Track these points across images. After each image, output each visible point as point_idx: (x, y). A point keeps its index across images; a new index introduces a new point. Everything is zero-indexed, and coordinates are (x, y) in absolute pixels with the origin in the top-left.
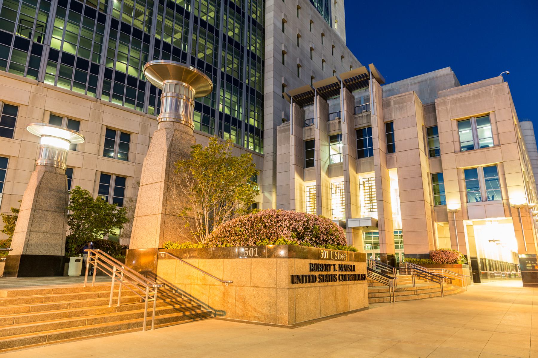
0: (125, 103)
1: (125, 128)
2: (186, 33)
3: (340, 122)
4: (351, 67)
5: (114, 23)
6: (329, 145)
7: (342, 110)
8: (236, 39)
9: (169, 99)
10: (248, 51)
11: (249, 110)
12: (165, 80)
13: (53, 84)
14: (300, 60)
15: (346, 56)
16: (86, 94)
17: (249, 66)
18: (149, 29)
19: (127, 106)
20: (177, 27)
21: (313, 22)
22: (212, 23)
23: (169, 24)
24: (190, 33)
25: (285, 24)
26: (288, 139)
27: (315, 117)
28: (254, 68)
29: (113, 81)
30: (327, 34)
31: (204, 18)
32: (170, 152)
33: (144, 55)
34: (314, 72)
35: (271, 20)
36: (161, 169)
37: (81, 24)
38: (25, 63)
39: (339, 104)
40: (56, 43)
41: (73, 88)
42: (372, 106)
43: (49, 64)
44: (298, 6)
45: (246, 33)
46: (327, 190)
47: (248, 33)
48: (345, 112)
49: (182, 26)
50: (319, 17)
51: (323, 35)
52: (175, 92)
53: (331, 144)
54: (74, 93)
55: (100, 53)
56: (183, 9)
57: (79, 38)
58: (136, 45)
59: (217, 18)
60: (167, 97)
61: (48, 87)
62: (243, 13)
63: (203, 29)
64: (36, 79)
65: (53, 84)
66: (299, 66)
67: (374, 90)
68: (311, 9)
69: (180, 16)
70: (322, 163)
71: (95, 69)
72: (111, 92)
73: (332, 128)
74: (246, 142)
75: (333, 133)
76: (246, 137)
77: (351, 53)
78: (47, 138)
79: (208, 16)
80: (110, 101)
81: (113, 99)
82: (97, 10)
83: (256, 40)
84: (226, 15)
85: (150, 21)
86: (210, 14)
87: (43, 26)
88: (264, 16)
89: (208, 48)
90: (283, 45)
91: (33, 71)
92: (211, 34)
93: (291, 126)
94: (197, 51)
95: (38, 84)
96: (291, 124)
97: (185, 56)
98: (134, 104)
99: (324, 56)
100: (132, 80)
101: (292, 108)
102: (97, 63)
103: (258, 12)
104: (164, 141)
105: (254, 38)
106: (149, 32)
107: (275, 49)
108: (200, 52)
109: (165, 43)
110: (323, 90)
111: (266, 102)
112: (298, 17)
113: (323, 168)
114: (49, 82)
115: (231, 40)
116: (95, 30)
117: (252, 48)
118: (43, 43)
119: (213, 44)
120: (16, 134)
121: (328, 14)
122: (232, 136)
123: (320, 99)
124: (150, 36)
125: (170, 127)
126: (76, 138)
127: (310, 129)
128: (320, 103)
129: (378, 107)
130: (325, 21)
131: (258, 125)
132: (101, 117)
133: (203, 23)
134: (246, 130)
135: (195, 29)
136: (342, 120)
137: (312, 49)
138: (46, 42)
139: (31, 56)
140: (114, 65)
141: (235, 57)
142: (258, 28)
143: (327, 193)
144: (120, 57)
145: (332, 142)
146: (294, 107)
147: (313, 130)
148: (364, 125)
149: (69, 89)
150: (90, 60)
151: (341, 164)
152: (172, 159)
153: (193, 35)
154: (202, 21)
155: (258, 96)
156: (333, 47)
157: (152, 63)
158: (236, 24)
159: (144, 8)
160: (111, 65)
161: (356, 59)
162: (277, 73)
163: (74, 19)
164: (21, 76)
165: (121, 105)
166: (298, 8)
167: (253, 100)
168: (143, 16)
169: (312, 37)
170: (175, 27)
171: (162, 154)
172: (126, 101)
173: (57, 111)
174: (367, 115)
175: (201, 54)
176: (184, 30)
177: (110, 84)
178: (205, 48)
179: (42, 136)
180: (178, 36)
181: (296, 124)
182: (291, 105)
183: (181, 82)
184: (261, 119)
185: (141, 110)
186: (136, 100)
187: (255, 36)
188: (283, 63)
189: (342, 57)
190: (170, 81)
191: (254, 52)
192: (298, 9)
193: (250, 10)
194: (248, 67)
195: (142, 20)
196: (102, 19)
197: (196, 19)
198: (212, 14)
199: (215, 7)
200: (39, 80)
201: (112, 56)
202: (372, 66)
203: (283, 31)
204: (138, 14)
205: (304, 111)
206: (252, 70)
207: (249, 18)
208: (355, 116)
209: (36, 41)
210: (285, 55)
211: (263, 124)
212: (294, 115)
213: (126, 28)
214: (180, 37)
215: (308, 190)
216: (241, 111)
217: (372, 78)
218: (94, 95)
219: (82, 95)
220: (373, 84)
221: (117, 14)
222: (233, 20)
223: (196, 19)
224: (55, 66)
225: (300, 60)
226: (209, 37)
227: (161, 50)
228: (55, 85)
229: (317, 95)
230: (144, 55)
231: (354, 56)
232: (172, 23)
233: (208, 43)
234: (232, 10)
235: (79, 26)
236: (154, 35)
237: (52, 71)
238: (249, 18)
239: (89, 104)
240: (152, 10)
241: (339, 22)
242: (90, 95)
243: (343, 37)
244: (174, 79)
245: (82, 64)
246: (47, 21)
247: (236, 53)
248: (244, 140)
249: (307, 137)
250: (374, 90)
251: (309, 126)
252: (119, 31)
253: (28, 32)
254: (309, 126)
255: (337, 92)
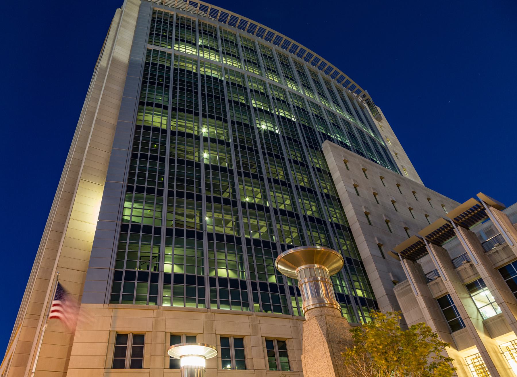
0: (232, 307)
1: (238, 333)
2: (270, 225)
3: (471, 265)
4: (443, 206)
5: (210, 236)
6: (471, 297)
7: (468, 251)
8: (316, 215)
9: (307, 285)
11: (352, 282)
12: (298, 267)
13: (169, 305)
14: (386, 216)
15: (431, 197)
16: (197, 307)
19: (235, 309)
20: (261, 223)
21: (383, 178)
24: (274, 225)
25: (358, 188)
26: (415, 302)
28: (342, 237)
29: (218, 288)
30: (402, 183)
32: (329, 342)
33: (239, 256)
35: (342, 189)
37: (185, 246)
38: (146, 292)
39: (460, 244)
40: (168, 268)
41: (186, 304)
43: (165, 288)
46: (498, 357)
47: (326, 207)
48: (473, 252)
49: (265, 221)
50: (387, 172)
51: (398, 185)
52: (311, 276)
53: (472, 295)
54: (188, 308)
55: (203, 265)
57: (185, 257)
58: (231, 249)
59: (293, 203)
60: (305, 283)
61: (166, 309)
62: (315, 192)
63: (285, 217)
64: (156, 304)
65: (169, 305)
66: (387, 222)
67: (498, 218)
68: (376, 167)
70: (474, 321)
72: (218, 299)
73: (464, 276)
74: (361, 318)
75: (468, 281)
76: (359, 312)
77: (436, 193)
78: (186, 357)
80: (219, 308)
81: (221, 306)
82: (195, 230)
83: (335, 211)
84: (301, 198)
85: (238, 225)
86: (286, 203)
87: (156, 257)
88: (335, 188)
89: (293, 232)
90: (363, 207)
91: (154, 298)
92: (292, 219)
93: (412, 286)
94: (284, 238)
95: (158, 309)
96: (410, 282)
98: (240, 305)
99: (409, 204)
100: (234, 282)
101: (406, 266)
102: (202, 275)
104: (318, 331)
105: (333, 210)
106: (239, 234)
107: (356, 214)
108: (286, 238)
109: (255, 240)
111: (367, 268)
112: (367, 178)
113: (477, 327)
114: (166, 305)
115: (311, 219)
116: (196, 247)
117: (334, 219)
118: (158, 271)
119: (296, 227)
120: (145, 364)
121: (393, 166)
122: (344, 315)
124: (240, 238)
125: (319, 314)
126: (210, 352)
127: (436, 283)
128: (436, 251)
130: (393, 172)
131: (367, 295)
132: (214, 327)
133: (283, 212)
134: (357, 304)
135: (277, 220)
136: (474, 262)
137: (393, 202)
138: (160, 270)
139: (151, 285)
141: (321, 233)
142: (333, 200)
144: (220, 265)
145: (472, 292)
146: (406, 264)
147: (441, 284)
148: (506, 261)
150: (196, 274)
152: (334, 350)
153: (277, 225)
154: (281, 210)
156: (414, 193)
157: (283, 255)
159: (230, 216)
160: (213, 274)
161: (444, 197)
163: (179, 244)
164: (144, 305)
165: (229, 309)
166: (364, 171)
167: (352, 269)
168: (231, 223)
170: (260, 224)
173: (176, 330)
174: (503, 249)
176: (268, 223)
177: (216, 291)
178: (291, 233)
179: (181, 357)
180: (264, 230)
182: (401, 262)
183: (312, 265)
184: (368, 287)
185: (247, 310)
186: (241, 301)
187: (333, 208)
188: (370, 224)
189: (429, 199)
191: (337, 222)
192: (364, 172)
193: (320, 187)
194: (336, 239)
195: (232, 226)
196: (200, 236)
197: (275, 210)
198: (288, 202)
199: (288, 195)
200: (159, 305)
201: (214, 265)
203: (358, 195)
204: (227, 222)
207: (322, 194)
209: (152, 270)
210: (369, 216)
211: (372, 292)
213: (220, 237)
214: (266, 230)
215: (469, 362)
216: (344, 284)
217: (488, 207)
218: (204, 306)
220: (492, 213)
221: (211, 229)
222: (308, 200)
223: (275, 210)
225: (386, 216)
226: (292, 222)
227: (253, 247)
228: (172, 305)
229: (428, 243)
230: (239, 256)
231: (440, 195)
232: (256, 221)
233: (291, 228)
234: (305, 193)
235: (183, 248)
236: (244, 236)
237: (167, 294)
238: (322, 194)
239: (202, 317)
240: (238, 216)
241: (407, 170)
242: (201, 306)
243: (419, 181)
244: (307, 264)
245: (191, 279)
247: (320, 229)
248: (359, 317)
250: (498, 218)
251: (432, 280)
252: (215, 242)
253: (146, 265)
254: (432, 280)
255: (451, 233)
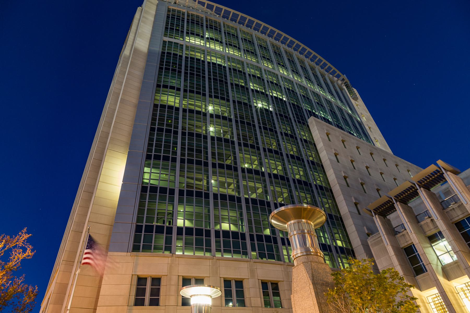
0: (234, 255)
2: (265, 187)
3: (432, 220)
4: (408, 171)
6: (432, 246)
7: (429, 208)
8: (303, 179)
9: (296, 236)
10: (316, 185)
13: (181, 253)
15: (399, 163)
17: (320, 197)
18: (239, 193)
19: (236, 256)
20: (258, 185)
22: (281, 173)
23: (252, 185)
24: (268, 186)
25: (338, 156)
27: (404, 222)
30: (374, 152)
31: (275, 172)
34: (377, 185)
35: (325, 157)
36: (312, 303)
37: (194, 204)
40: (180, 222)
41: (195, 252)
42: (459, 196)
43: (177, 239)
44: (342, 140)
45: (310, 173)
46: (454, 296)
47: (311, 172)
48: (434, 209)
49: (261, 183)
50: (363, 143)
51: (371, 154)
52: (299, 229)
53: (433, 245)
54: (197, 256)
55: (209, 220)
56: (259, 171)
57: (194, 214)
58: (233, 207)
59: (284, 169)
60: (294, 235)
61: (179, 257)
62: (303, 160)
63: (277, 181)
64: (171, 253)
65: (181, 253)
68: (353, 139)
69: (258, 177)
70: (434, 267)
71: (208, 233)
72: (222, 249)
73: (426, 229)
74: (341, 264)
75: (430, 233)
76: (339, 259)
77: (403, 160)
78: (196, 297)
79: (277, 170)
82: (203, 191)
85: (238, 187)
87: (171, 213)
90: (342, 172)
94: (277, 198)
96: (381, 234)
97: (268, 204)
98: (240, 253)
99: (381, 169)
100: (235, 234)
101: (377, 220)
102: (208, 228)
103: (313, 155)
105: (317, 174)
106: (239, 194)
109: (252, 199)
110: (400, 196)
112: (345, 148)
114: (179, 253)
115: (299, 181)
117: (318, 182)
120: (161, 302)
123: (401, 205)
125: (306, 261)
127: (403, 235)
129: (467, 195)
130: (368, 143)
132: (218, 272)
133: (276, 176)
134: (337, 252)
136: (434, 217)
137: (367, 168)
138: (174, 224)
140: (221, 227)
142: (318, 166)
143: (456, 300)
144: (223, 220)
145: (433, 242)
148: (461, 216)
149: (193, 254)
150: (203, 227)
151: (455, 263)
152: (319, 291)
153: (271, 187)
154: (274, 174)
155: (337, 219)
156: (384, 160)
157: (276, 211)
158: (300, 169)
159: (232, 179)
160: (218, 227)
161: (410, 163)
162: (347, 197)
163: (189, 202)
166: (343, 142)
168: (233, 185)
169: (363, 159)
171: (308, 288)
172: (234, 253)
174: (459, 206)
175: (280, 198)
177: (220, 242)
178: (282, 193)
179: (191, 296)
181: (387, 234)
182: (374, 218)
183: (300, 220)
184: (346, 238)
185: (246, 257)
187: (317, 172)
188: (348, 186)
189: (397, 165)
190: (292, 222)
191: (320, 184)
192: (343, 143)
193: (306, 155)
196: (207, 196)
197: (269, 175)
198: (280, 168)
199: (280, 162)
201: (218, 221)
202: (440, 162)
203: (338, 162)
204: (229, 184)
205: (389, 220)
206: (323, 199)
207: (308, 161)
208: (445, 211)
209: (167, 224)
210: (347, 179)
211: (350, 243)
212: (381, 226)
213: (223, 197)
214: (262, 191)
215: (431, 301)
216: (326, 236)
217: (446, 172)
219: (202, 257)
220: (450, 177)
222: (297, 166)
223: (269, 175)
224: (182, 239)
225: (361, 179)
227: (251, 205)
228: (183, 253)
234: (294, 160)
236: (243, 196)
238: (308, 161)
239: (209, 263)
241: (379, 141)
242: (208, 254)
243: (389, 151)
244: (295, 219)
245: (199, 232)
246: (173, 209)
248: (339, 263)
249: (404, 244)
250: (454, 181)
251: (399, 233)
252: (219, 200)
254: (399, 233)
